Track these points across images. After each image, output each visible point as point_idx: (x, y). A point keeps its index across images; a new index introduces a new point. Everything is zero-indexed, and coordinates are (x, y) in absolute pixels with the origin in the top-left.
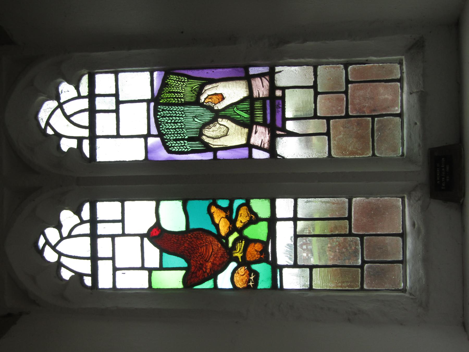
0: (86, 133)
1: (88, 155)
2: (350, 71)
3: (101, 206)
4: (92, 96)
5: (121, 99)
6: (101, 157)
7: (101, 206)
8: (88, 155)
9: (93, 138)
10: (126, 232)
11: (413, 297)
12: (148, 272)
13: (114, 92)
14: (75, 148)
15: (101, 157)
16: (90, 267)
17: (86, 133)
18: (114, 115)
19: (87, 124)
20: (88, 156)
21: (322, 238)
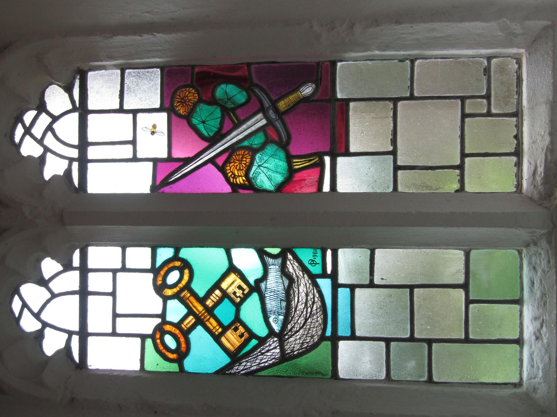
0: (74, 153)
1: (77, 358)
2: (418, 66)
3: (92, 251)
4: (84, 270)
5: (119, 266)
6: (93, 188)
7: (92, 251)
8: (77, 358)
9: (83, 161)
10: (131, 138)
11: (534, 303)
12: (167, 115)
13: (110, 274)
14: (60, 175)
15: (93, 188)
16: (78, 343)
17: (74, 153)
18: (110, 331)
19: (76, 143)
20: (77, 186)
21: (376, 342)
